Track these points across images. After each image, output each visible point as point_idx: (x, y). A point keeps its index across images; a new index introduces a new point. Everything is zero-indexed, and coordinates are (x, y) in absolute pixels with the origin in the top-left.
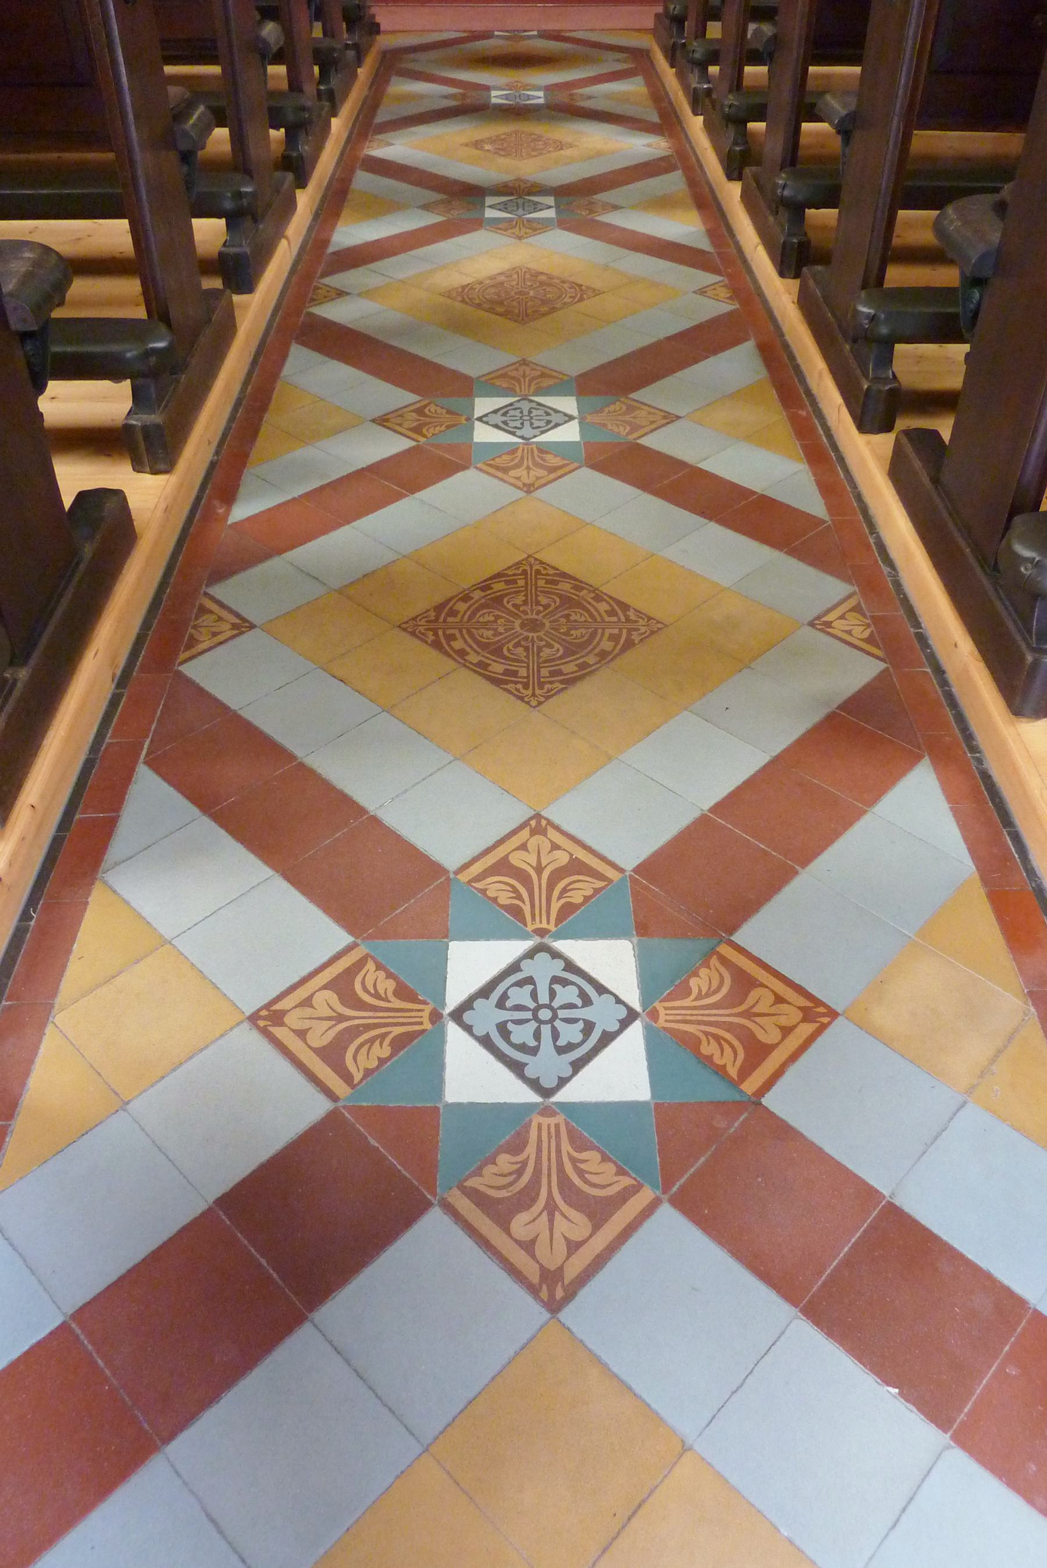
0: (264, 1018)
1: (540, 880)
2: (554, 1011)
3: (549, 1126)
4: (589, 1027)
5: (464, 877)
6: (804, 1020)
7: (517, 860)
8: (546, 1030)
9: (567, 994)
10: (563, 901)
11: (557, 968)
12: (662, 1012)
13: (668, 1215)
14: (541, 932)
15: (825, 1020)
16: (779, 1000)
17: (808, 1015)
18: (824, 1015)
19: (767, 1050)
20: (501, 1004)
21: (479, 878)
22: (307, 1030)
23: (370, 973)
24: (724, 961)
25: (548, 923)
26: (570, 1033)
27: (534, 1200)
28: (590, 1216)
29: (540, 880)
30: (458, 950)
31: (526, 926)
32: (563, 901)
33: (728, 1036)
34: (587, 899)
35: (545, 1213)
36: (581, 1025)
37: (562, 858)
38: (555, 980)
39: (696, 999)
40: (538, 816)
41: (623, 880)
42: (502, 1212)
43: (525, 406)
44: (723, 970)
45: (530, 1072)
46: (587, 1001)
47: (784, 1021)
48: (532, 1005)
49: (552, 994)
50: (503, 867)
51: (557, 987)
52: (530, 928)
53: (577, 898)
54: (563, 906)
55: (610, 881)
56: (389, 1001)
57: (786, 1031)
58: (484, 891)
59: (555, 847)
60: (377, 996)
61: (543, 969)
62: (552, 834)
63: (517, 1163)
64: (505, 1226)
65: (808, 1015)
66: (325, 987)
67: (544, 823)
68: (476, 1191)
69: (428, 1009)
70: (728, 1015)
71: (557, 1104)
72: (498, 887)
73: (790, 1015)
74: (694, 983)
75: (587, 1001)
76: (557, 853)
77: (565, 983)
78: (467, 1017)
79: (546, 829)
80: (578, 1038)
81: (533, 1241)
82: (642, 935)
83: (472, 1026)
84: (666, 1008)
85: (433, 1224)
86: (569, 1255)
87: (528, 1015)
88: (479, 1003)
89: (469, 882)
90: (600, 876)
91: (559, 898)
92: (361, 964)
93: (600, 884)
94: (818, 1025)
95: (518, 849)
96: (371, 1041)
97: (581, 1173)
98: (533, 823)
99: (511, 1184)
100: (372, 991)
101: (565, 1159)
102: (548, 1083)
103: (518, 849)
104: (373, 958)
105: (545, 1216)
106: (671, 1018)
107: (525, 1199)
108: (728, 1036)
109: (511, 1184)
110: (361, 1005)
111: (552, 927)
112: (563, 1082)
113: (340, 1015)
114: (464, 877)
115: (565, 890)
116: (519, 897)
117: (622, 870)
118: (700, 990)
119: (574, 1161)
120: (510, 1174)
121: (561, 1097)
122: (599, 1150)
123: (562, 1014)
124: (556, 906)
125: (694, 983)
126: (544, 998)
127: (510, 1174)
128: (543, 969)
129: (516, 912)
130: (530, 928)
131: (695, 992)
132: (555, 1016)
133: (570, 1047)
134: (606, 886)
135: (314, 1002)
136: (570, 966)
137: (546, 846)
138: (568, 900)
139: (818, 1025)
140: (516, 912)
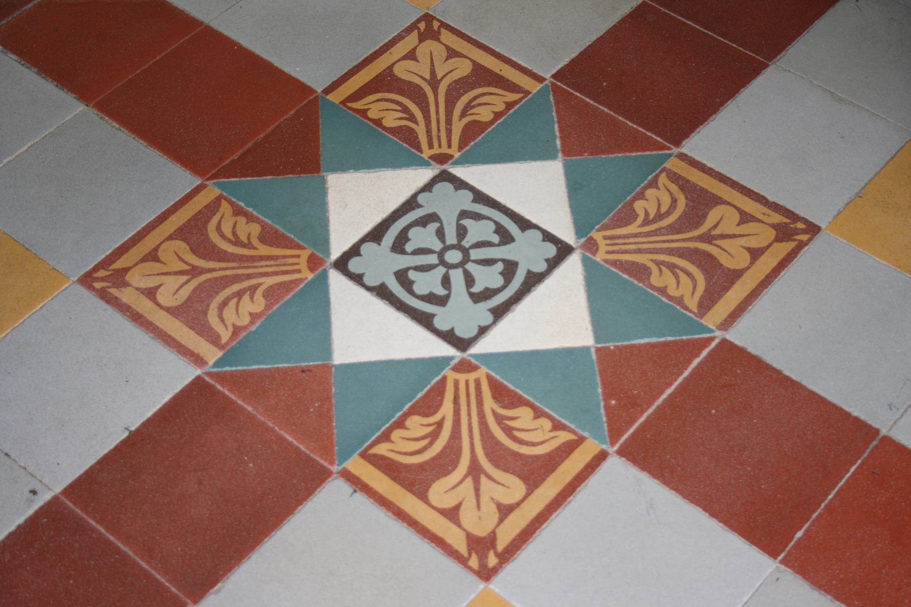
0: (102, 279)
1: (473, 451)
2: (465, 252)
3: (467, 382)
4: (510, 268)
5: (336, 97)
6: (778, 240)
7: (510, 488)
8: (451, 238)
9: (478, 231)
10: (437, 417)
11: (443, 318)
12: (602, 243)
13: (616, 467)
14: (441, 159)
15: (804, 237)
16: (746, 218)
17: (783, 233)
18: (804, 232)
19: (181, 234)
20: (399, 246)
21: (569, 448)
22: (157, 288)
23: (225, 219)
24: (675, 178)
25: (450, 146)
26: (423, 237)
27: (455, 464)
28: (525, 479)
29: (473, 451)
30: (581, 335)
31: (421, 152)
32: (437, 417)
33: (231, 249)
34: (400, 424)
35: (439, 77)
36: (500, 266)
37: (463, 69)
38: (442, 301)
39: (642, 225)
40: (486, 574)
41: (345, 456)
42: (416, 479)
43: (447, 204)
44: (674, 188)
45: (441, 323)
46: (402, 276)
47: (755, 243)
48: (470, 267)
49: (446, 282)
50: (534, 472)
51: (441, 291)
52: (427, 153)
53: (484, 114)
54: (435, 412)
55: (527, 93)
56: (255, 248)
57: (755, 254)
58: (558, 426)
59: (452, 53)
60: (672, 267)
61: (447, 204)
62: (446, 36)
63: (429, 425)
64: (423, 496)
65: (783, 233)
66: (170, 238)
67: (474, 562)
68: (383, 458)
69: (305, 254)
70: (213, 270)
71: (476, 356)
72: (536, 435)
73: (761, 235)
74: (639, 206)
75: (402, 276)
76: (448, 502)
77: (430, 298)
78: (354, 265)
79: (439, 32)
80: (499, 281)
81: (458, 507)
82: (568, 155)
83: (544, 240)
84: (605, 238)
85: (333, 495)
86: (501, 521)
87: (475, 254)
88: (542, 267)
89: (343, 103)
90: (512, 87)
91: (443, 419)
92: (213, 208)
93: (512, 97)
94: (796, 243)
95: (404, 58)
96: (239, 295)
97: (508, 431)
98: (492, 561)
99: (425, 449)
100: (678, 271)
101: (491, 420)
102: (463, 332)
103: (404, 58)
104: (226, 199)
105: (469, 481)
106: (291, 261)
107: (444, 464)
108: (231, 249)
109: (425, 449)
110: (224, 257)
111: (451, 376)
112: (427, 187)
113: (194, 267)
114: (336, 97)
115: (434, 436)
116: (412, 118)
117: (348, 476)
118: (647, 213)
119: (499, 419)
120: (423, 438)
121: (479, 348)
122: (385, 128)
123: (433, 259)
124: (458, 127)
125: (639, 206)
126: (457, 276)
127: (423, 438)
128: (460, 314)
129: (501, 393)
130: (427, 153)
131: (259, 294)
132: (441, 254)
133: (488, 294)
134: (521, 99)
135: (160, 254)
136: (480, 197)
137: (468, 516)
138: (426, 421)
139: (796, 243)
140: (501, 393)
